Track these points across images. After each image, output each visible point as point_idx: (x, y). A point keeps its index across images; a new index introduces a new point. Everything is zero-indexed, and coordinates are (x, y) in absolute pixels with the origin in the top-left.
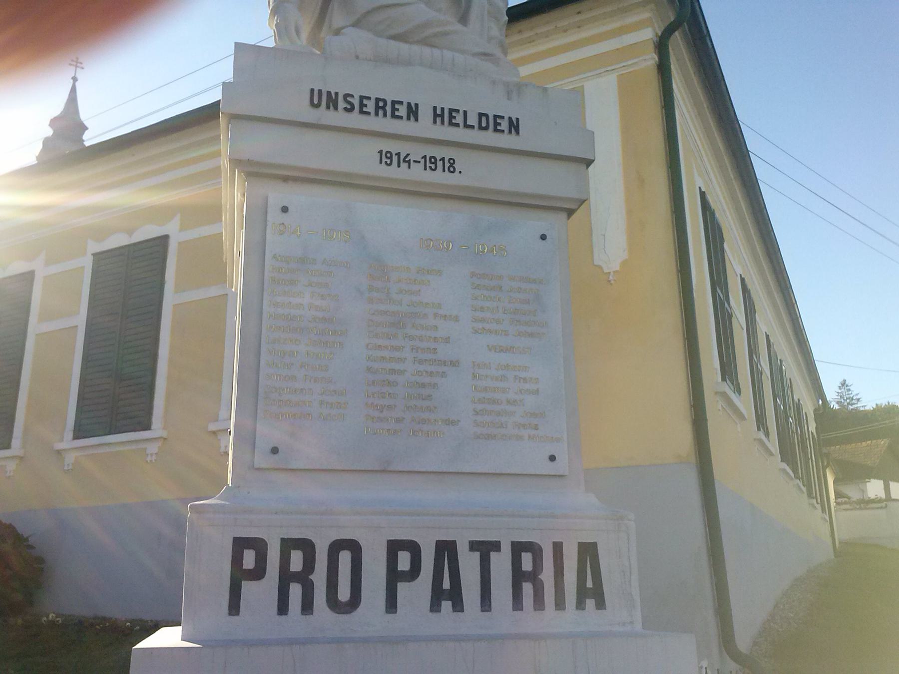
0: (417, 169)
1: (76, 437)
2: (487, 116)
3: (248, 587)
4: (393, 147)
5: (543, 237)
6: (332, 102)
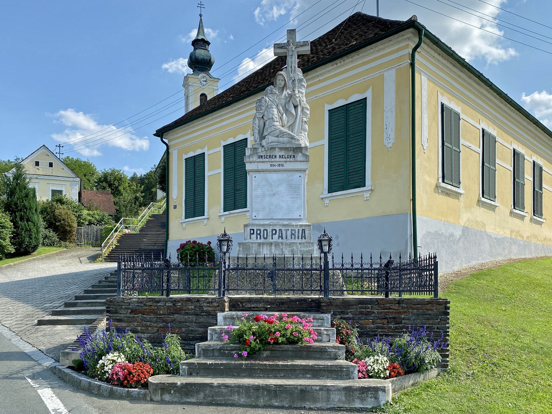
1: (224, 211)
5: (300, 176)
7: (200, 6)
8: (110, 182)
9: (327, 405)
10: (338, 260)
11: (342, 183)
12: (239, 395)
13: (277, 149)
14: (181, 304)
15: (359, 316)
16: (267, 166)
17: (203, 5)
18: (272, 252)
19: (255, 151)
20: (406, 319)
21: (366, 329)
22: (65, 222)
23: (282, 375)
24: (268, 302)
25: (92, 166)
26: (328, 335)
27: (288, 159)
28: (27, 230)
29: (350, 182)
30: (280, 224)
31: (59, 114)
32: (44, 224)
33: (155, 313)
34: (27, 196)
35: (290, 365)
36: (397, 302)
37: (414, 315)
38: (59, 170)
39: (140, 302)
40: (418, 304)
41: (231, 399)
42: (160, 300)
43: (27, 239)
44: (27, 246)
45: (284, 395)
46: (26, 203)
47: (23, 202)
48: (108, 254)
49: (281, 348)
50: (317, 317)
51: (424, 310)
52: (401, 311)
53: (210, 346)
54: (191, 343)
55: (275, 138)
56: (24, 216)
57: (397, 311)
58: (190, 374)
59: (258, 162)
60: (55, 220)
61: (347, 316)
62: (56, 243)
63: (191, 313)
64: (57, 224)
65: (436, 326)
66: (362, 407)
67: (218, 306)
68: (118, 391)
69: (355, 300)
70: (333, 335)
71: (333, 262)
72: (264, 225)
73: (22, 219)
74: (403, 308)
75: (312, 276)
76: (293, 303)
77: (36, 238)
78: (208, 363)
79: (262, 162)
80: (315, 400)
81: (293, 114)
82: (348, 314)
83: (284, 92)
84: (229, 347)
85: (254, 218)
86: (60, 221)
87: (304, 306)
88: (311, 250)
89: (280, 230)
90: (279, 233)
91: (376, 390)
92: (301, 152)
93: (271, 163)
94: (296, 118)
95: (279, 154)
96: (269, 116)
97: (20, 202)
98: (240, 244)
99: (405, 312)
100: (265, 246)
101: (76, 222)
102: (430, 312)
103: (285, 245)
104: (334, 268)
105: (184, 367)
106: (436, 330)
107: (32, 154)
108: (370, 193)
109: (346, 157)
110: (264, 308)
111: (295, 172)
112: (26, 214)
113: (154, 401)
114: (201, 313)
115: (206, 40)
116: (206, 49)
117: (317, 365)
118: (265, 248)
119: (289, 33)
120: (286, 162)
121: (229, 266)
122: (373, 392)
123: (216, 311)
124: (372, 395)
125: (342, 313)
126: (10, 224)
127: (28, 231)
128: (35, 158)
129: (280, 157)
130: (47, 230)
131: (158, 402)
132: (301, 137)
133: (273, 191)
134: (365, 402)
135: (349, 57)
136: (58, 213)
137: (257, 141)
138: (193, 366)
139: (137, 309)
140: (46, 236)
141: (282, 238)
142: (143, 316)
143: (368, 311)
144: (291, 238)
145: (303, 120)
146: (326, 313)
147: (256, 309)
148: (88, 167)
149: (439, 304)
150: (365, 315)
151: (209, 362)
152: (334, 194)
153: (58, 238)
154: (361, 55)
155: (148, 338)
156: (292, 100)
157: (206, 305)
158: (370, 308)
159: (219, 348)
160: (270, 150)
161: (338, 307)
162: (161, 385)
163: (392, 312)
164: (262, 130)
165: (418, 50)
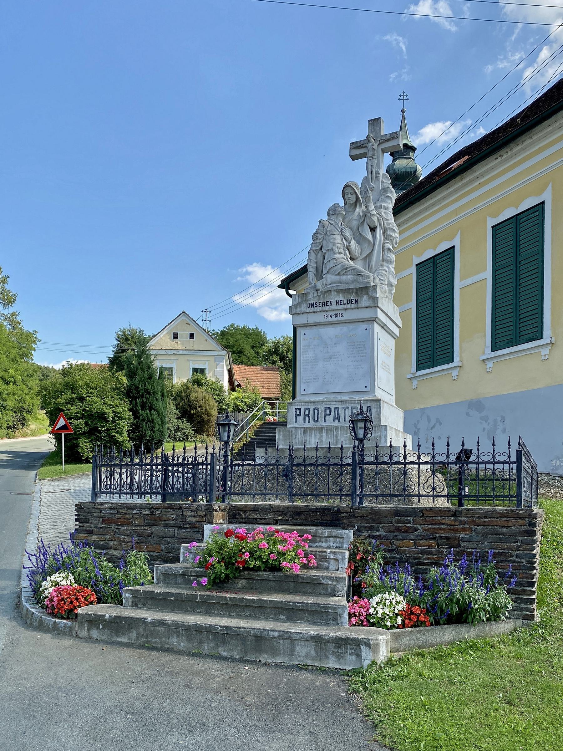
0: (333, 318)
5: (366, 329)
7: (402, 98)
8: (282, 354)
9: (290, 660)
11: (512, 336)
12: (178, 636)
13: (333, 292)
16: (320, 318)
17: (406, 96)
18: (322, 440)
20: (466, 540)
22: (202, 409)
23: (248, 614)
24: (279, 511)
25: (262, 334)
26: (336, 560)
27: (349, 306)
28: (149, 421)
29: (522, 334)
30: (337, 399)
31: (244, 270)
32: (177, 412)
33: (130, 524)
34: (150, 378)
35: (257, 599)
36: (452, 513)
37: (479, 534)
38: (201, 342)
39: (114, 507)
40: (485, 517)
41: (168, 642)
43: (149, 433)
44: (149, 441)
45: (235, 642)
46: (149, 386)
47: (145, 386)
48: (239, 450)
49: (259, 575)
50: (334, 534)
51: (496, 527)
52: (459, 527)
53: (171, 569)
55: (336, 277)
56: (146, 403)
57: (452, 527)
58: (135, 605)
59: (308, 313)
60: (190, 407)
61: (378, 533)
62: (190, 437)
63: (172, 525)
64: (192, 411)
65: (514, 553)
66: (338, 667)
67: (205, 516)
68: (47, 621)
69: (389, 510)
70: (343, 561)
73: (143, 407)
74: (461, 523)
76: (312, 514)
77: (160, 431)
78: (156, 591)
79: (314, 312)
80: (275, 652)
81: (369, 241)
82: (378, 531)
83: (357, 210)
84: (194, 572)
86: (196, 408)
87: (328, 518)
88: (377, 436)
90: (335, 413)
91: (357, 643)
93: (326, 313)
94: (374, 247)
95: (336, 299)
96: (328, 247)
97: (141, 386)
99: (464, 530)
100: (313, 431)
101: (216, 408)
102: (504, 530)
103: (340, 430)
105: (127, 595)
106: (514, 559)
107: (169, 324)
108: (550, 348)
109: (516, 295)
110: (274, 520)
111: (359, 323)
112: (149, 400)
113: (79, 637)
114: (184, 524)
115: (410, 145)
116: (410, 158)
117: (293, 603)
118: (313, 435)
119: (371, 124)
120: (346, 309)
122: (354, 647)
123: (202, 523)
124: (353, 651)
125: (370, 528)
126: (127, 414)
127: (150, 421)
128: (172, 329)
129: (337, 303)
130: (179, 420)
131: (84, 638)
132: (382, 272)
133: (328, 353)
134: (342, 661)
135: (518, 143)
136: (193, 398)
137: (312, 284)
138: (138, 595)
139: (110, 518)
140: (178, 428)
141: (339, 421)
142: (116, 527)
143: (408, 527)
145: (386, 247)
146: (347, 529)
147: (263, 521)
148: (256, 335)
149: (520, 517)
150: (403, 532)
151: (169, 590)
152: (499, 353)
153: (193, 430)
154: (535, 138)
156: (367, 220)
157: (190, 514)
158: (412, 522)
159: (182, 572)
160: (324, 295)
161: (363, 519)
162: (87, 616)
163: (445, 529)
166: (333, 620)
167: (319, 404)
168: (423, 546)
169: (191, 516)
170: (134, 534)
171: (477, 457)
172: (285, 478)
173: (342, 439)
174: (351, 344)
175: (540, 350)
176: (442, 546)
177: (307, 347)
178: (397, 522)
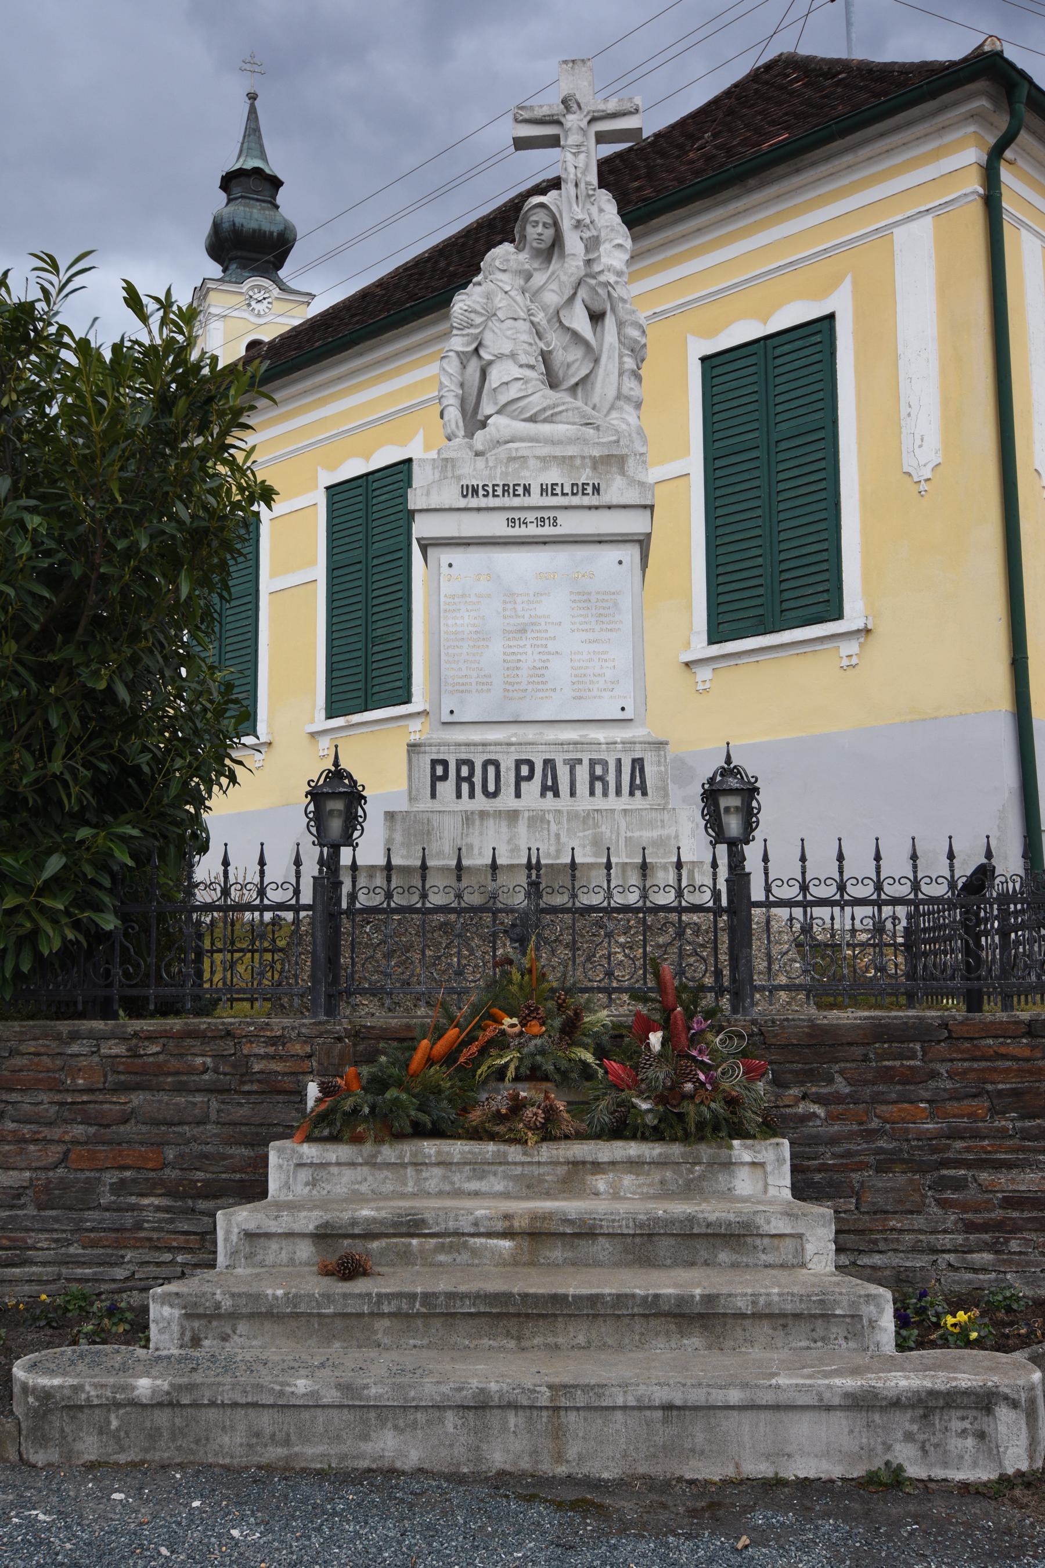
1: (329, 717)
2: (577, 485)
3: (440, 786)
4: (516, 515)
5: (620, 562)
6: (475, 491)
10: (784, 866)
14: (158, 1049)
15: (875, 1088)
16: (496, 526)
19: (449, 468)
21: (908, 1140)
23: (581, 1339)
36: (1023, 1029)
42: (77, 1031)
54: (203, 1205)
55: (523, 424)
67: (309, 1056)
71: (766, 874)
72: (484, 745)
75: (680, 934)
78: (270, 1292)
85: (446, 717)
89: (546, 762)
92: (622, 472)
93: (511, 515)
98: (390, 816)
103: (568, 820)
104: (772, 898)
114: (244, 1083)
115: (268, 171)
121: (353, 897)
123: (300, 1078)
129: (543, 490)
141: (556, 794)
143: (910, 1067)
144: (592, 793)
155: (25, 1188)
157: (262, 1051)
158: (920, 1054)
163: (1008, 1070)
164: (472, 399)
165: (1008, 154)
166: (846, 1338)
167: (498, 748)
168: (954, 1116)
169: (266, 1057)
170: (72, 1116)
171: (838, 889)
172: (517, 945)
173: (575, 843)
174: (580, 597)
175: (836, 644)
176: (1004, 1113)
177: (456, 600)
178: (881, 1057)
